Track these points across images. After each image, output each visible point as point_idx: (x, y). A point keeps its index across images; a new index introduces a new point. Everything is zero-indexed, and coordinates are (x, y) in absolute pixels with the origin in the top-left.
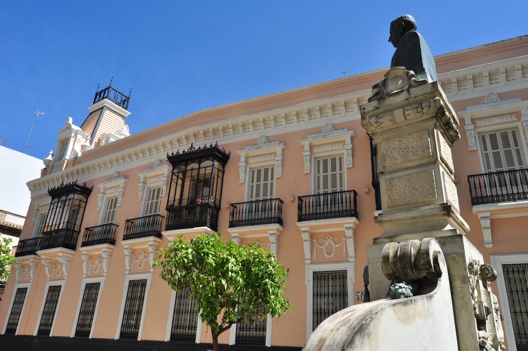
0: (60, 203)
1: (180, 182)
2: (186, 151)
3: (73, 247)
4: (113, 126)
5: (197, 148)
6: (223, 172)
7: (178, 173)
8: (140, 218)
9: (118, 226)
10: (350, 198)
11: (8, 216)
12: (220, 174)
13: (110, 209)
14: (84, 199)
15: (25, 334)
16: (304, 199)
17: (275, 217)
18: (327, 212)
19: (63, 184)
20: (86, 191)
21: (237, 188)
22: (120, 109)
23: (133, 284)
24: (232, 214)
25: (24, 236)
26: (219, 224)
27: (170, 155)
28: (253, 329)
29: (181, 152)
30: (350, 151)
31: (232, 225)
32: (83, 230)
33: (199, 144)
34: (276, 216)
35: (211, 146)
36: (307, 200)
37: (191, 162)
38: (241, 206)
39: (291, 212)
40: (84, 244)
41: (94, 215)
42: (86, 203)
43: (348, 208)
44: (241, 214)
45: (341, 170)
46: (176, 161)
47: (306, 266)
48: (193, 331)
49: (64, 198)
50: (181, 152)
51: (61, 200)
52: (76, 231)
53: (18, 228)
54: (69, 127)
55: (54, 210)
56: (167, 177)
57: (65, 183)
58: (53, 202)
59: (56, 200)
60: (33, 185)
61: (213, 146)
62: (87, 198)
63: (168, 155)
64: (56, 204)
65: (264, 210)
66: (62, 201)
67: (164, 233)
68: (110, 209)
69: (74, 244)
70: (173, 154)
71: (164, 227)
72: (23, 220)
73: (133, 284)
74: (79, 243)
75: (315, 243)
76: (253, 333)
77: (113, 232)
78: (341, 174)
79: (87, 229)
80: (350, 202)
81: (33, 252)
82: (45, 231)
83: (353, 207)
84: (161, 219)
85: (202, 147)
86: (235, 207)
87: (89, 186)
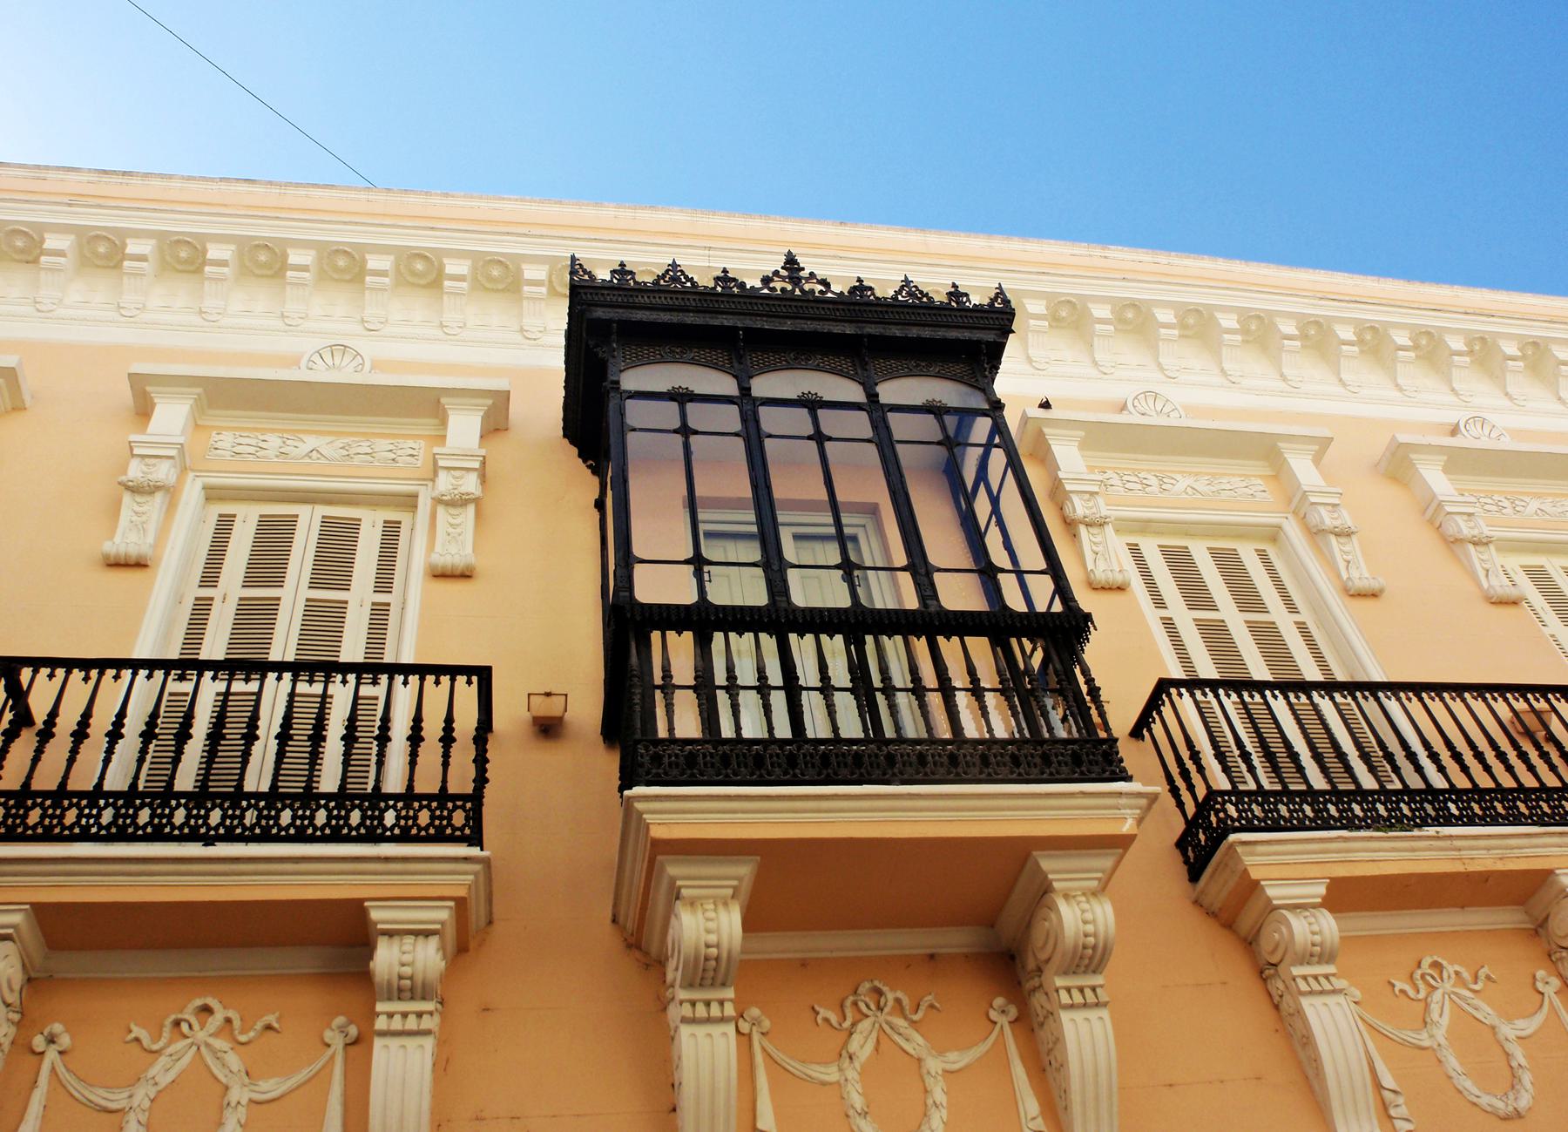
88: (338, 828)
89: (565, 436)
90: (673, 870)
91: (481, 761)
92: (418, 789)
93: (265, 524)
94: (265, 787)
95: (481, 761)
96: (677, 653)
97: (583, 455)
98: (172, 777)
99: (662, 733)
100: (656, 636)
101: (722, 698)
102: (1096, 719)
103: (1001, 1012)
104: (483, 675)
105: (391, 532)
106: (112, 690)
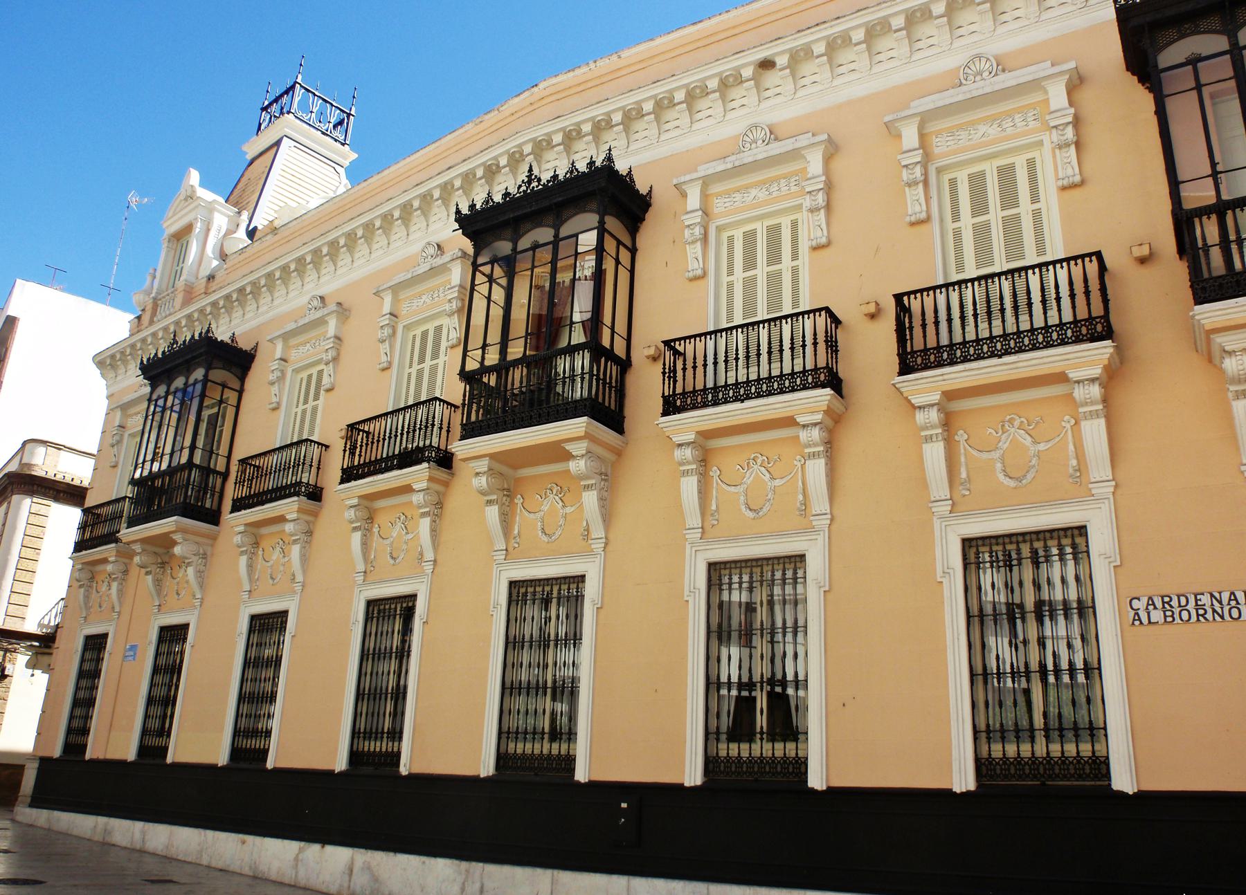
0: (170, 398)
1: (498, 294)
2: (513, 190)
3: (213, 517)
4: (305, 176)
5: (546, 177)
6: (633, 251)
7: (492, 262)
8: (386, 414)
9: (327, 447)
10: (1086, 280)
11: (64, 454)
12: (625, 256)
13: (306, 402)
14: (235, 384)
15: (110, 756)
16: (915, 305)
17: (816, 369)
18: (1005, 336)
19: (175, 342)
20: (237, 360)
21: (680, 290)
22: (327, 145)
23: (377, 610)
24: (670, 374)
25: (90, 501)
26: (628, 411)
27: (465, 210)
28: (762, 733)
29: (498, 198)
30: (1070, 133)
31: (671, 406)
32: (234, 468)
33: (554, 166)
34: (822, 363)
35: (592, 163)
36: (928, 301)
37: (528, 225)
38: (700, 345)
39: (871, 349)
40: (238, 505)
41: (264, 420)
42: (241, 392)
43: (1082, 314)
44: (700, 370)
45: (1035, 198)
46: (482, 225)
47: (937, 523)
48: (564, 747)
49: (179, 382)
50: (498, 198)
51: (172, 389)
52: (219, 473)
53: (77, 482)
54: (191, 197)
55: (157, 418)
56: (461, 286)
57: (180, 341)
58: (154, 397)
59: (161, 390)
60: (107, 362)
61: (598, 164)
62: (242, 378)
63: (458, 212)
64: (161, 402)
65: (775, 351)
66: (177, 390)
67: (461, 448)
68: (306, 402)
69: (215, 507)
70: (472, 206)
71: (457, 430)
72: (91, 463)
73: (377, 610)
74: (227, 504)
75: (963, 444)
76: (545, 747)
77: (315, 464)
78: (1037, 215)
79: (243, 462)
80: (1087, 293)
81: (111, 538)
82: (137, 475)
83: (1097, 310)
84: (447, 412)
85: (561, 174)
86: (676, 353)
87: (245, 345)
88: (1062, 340)
89: (1128, 70)
90: (1219, 340)
91: (1105, 301)
92: (1094, 315)
93: (971, 177)
94: (1071, 319)
95: (1105, 301)
96: (1210, 230)
97: (1142, 80)
98: (483, 358)
99: (1206, 275)
100: (1197, 221)
101: (1234, 247)
102: (167, 725)
103: (1081, 72)
104: (1098, 255)
105: (1031, 164)
106: (994, 288)
